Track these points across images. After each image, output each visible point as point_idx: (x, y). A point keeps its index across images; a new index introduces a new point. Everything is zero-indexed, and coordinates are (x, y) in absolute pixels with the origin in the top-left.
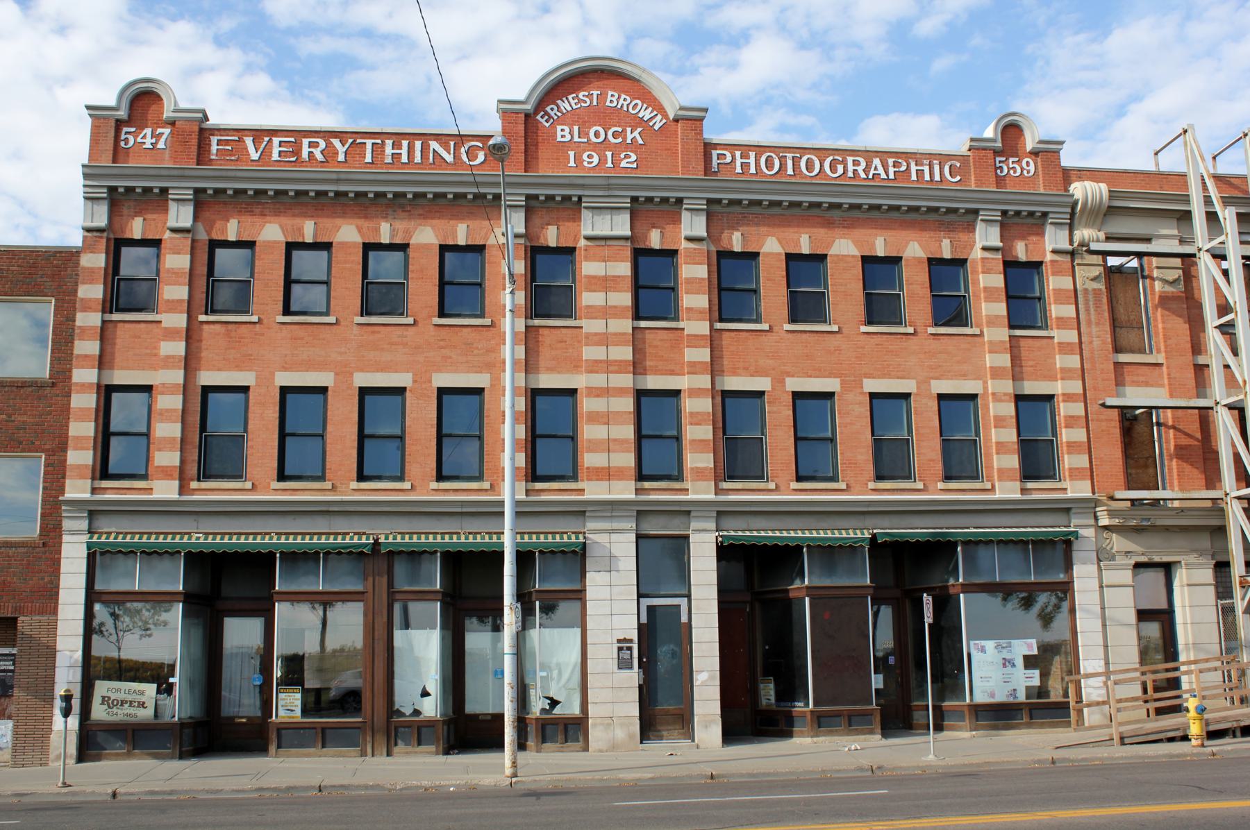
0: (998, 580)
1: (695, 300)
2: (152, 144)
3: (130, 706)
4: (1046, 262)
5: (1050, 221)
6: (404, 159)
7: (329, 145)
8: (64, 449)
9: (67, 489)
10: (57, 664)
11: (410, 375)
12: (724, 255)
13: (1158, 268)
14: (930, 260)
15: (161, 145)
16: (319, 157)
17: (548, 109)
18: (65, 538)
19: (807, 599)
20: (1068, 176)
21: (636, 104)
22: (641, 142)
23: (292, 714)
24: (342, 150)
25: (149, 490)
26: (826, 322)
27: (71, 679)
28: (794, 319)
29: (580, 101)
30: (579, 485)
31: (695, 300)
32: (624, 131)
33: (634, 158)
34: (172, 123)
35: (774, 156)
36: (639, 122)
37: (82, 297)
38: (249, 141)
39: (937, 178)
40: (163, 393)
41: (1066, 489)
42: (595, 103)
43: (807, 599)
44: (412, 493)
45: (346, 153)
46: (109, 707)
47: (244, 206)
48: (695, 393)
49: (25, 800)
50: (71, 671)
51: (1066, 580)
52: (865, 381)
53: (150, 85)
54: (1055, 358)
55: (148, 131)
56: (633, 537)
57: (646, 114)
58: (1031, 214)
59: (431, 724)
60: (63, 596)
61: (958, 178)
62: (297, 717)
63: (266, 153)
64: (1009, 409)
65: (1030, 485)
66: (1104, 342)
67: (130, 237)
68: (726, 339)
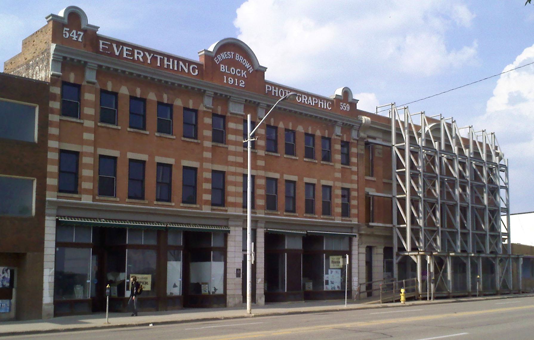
0: (74, 241)
2: (76, 38)
6: (171, 67)
7: (144, 54)
8: (45, 178)
9: (47, 196)
10: (44, 275)
12: (103, 92)
14: (184, 108)
15: (80, 40)
16: (141, 59)
17: (218, 56)
18: (47, 218)
21: (245, 61)
23: (206, 292)
24: (149, 58)
25: (226, 211)
26: (170, 134)
27: (50, 281)
28: (159, 131)
29: (228, 56)
30: (351, 219)
32: (241, 71)
33: (244, 83)
34: (85, 31)
35: (283, 90)
36: (245, 69)
38: (114, 46)
39: (325, 108)
40: (85, 156)
42: (232, 58)
45: (151, 59)
48: (88, 155)
50: (50, 278)
53: (78, 11)
57: (248, 66)
59: (176, 297)
60: (46, 244)
61: (330, 108)
63: (121, 52)
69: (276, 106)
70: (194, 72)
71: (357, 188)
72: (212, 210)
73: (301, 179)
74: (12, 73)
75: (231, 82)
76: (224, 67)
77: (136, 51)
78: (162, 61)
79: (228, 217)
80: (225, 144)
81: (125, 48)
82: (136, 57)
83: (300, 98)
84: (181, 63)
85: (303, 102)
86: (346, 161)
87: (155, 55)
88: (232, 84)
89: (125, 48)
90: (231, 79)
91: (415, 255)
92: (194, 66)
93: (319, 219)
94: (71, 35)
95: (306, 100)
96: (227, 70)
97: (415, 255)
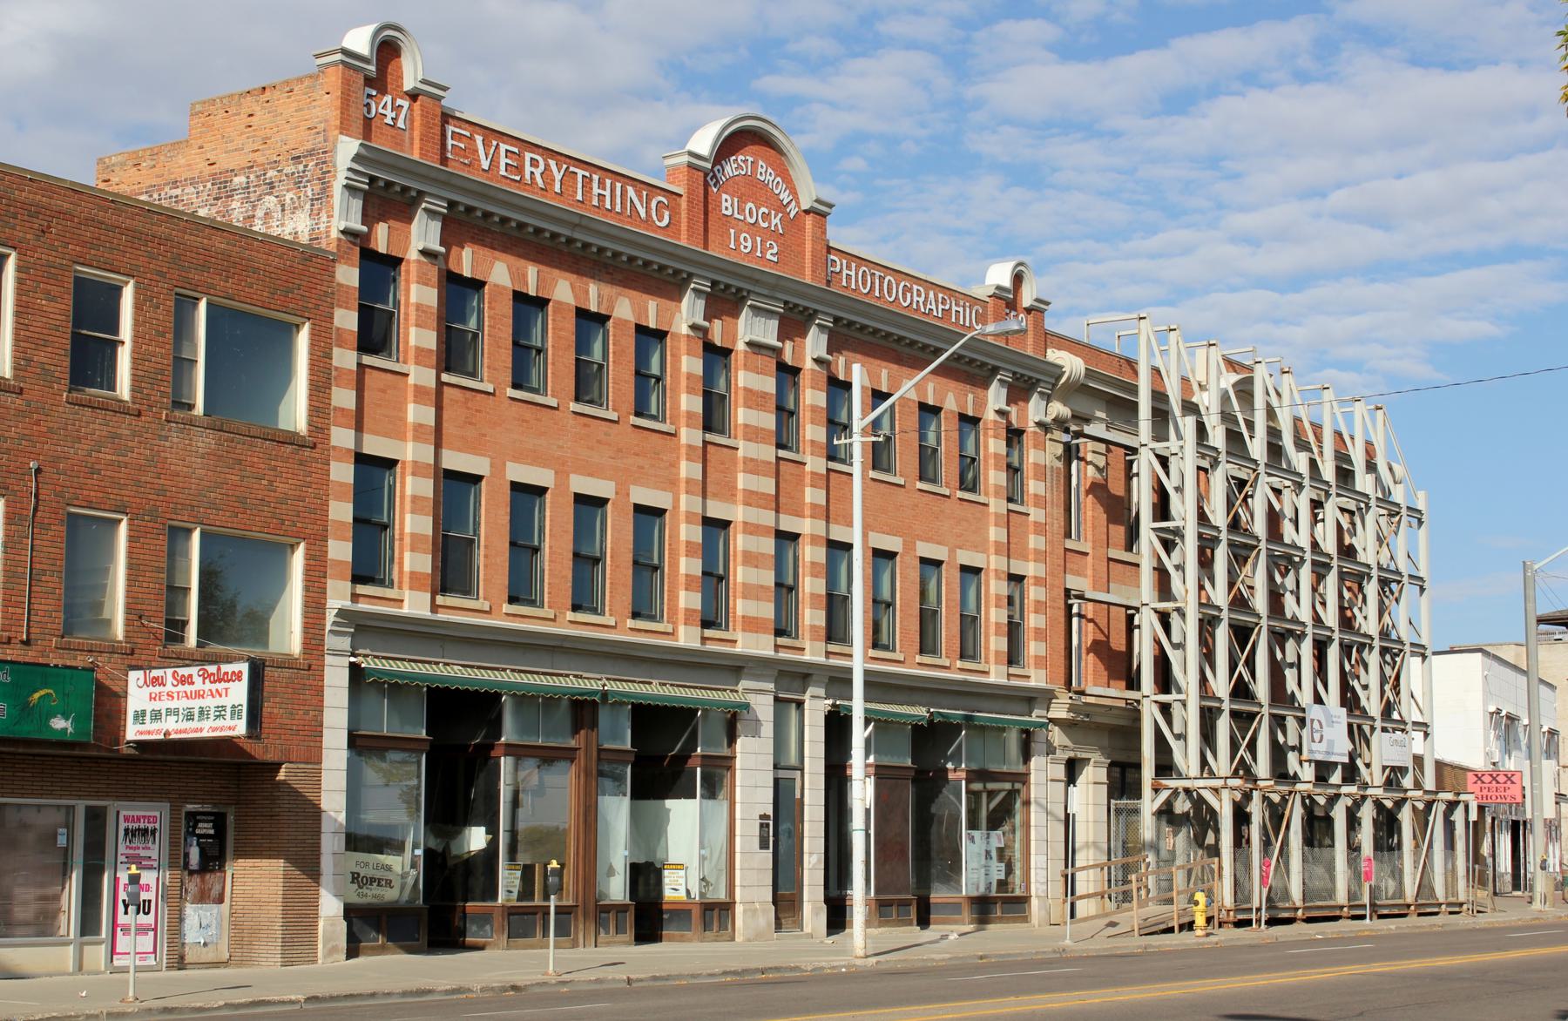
1: (418, 336)
3: (378, 885)
4: (408, 261)
5: (1039, 389)
7: (547, 166)
11: (612, 484)
13: (1094, 452)
18: (328, 659)
19: (699, 769)
20: (1048, 339)
22: (781, 231)
24: (558, 177)
27: (336, 849)
29: (739, 167)
31: (418, 336)
32: (769, 213)
33: (775, 250)
36: (782, 208)
37: (339, 326)
39: (968, 324)
41: (1029, 677)
43: (699, 769)
44: (613, 631)
46: (360, 887)
47: (476, 231)
49: (1447, 929)
50: (336, 838)
51: (729, 754)
52: (919, 544)
54: (804, 492)
55: (388, 98)
56: (771, 699)
57: (785, 197)
58: (984, 364)
62: (220, 914)
63: (494, 162)
64: (426, 488)
65: (362, 589)
66: (1060, 527)
67: (645, 324)
68: (371, 379)
69: (954, 353)
70: (661, 219)
71: (1068, 577)
72: (828, 654)
73: (909, 546)
74: (143, 198)
75: (746, 247)
76: (730, 202)
77: (528, 156)
78: (587, 181)
79: (806, 671)
80: (398, 361)
81: (503, 147)
82: (528, 176)
83: (909, 295)
84: (631, 191)
85: (915, 306)
86: (713, 415)
87: (572, 169)
88: (667, 226)
89: (503, 147)
90: (745, 239)
91: (1216, 790)
92: (661, 198)
93: (948, 668)
94: (381, 111)
95: (921, 300)
96: (736, 212)
97: (1216, 790)
